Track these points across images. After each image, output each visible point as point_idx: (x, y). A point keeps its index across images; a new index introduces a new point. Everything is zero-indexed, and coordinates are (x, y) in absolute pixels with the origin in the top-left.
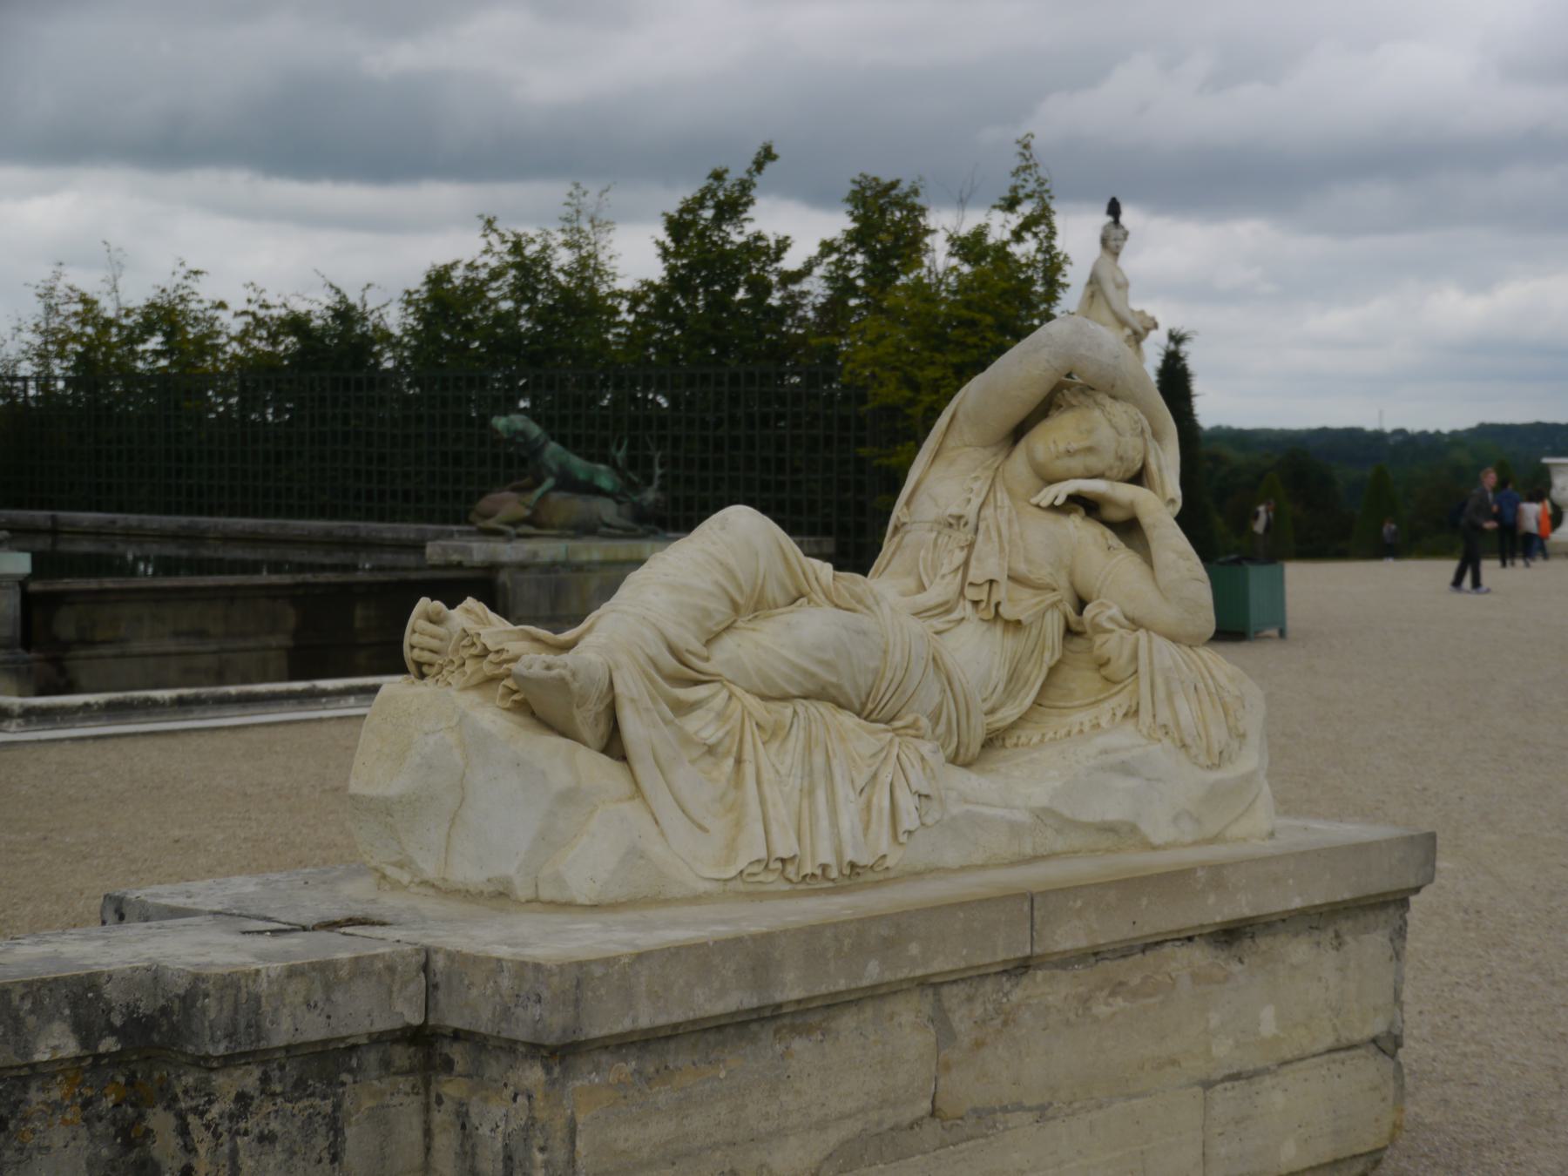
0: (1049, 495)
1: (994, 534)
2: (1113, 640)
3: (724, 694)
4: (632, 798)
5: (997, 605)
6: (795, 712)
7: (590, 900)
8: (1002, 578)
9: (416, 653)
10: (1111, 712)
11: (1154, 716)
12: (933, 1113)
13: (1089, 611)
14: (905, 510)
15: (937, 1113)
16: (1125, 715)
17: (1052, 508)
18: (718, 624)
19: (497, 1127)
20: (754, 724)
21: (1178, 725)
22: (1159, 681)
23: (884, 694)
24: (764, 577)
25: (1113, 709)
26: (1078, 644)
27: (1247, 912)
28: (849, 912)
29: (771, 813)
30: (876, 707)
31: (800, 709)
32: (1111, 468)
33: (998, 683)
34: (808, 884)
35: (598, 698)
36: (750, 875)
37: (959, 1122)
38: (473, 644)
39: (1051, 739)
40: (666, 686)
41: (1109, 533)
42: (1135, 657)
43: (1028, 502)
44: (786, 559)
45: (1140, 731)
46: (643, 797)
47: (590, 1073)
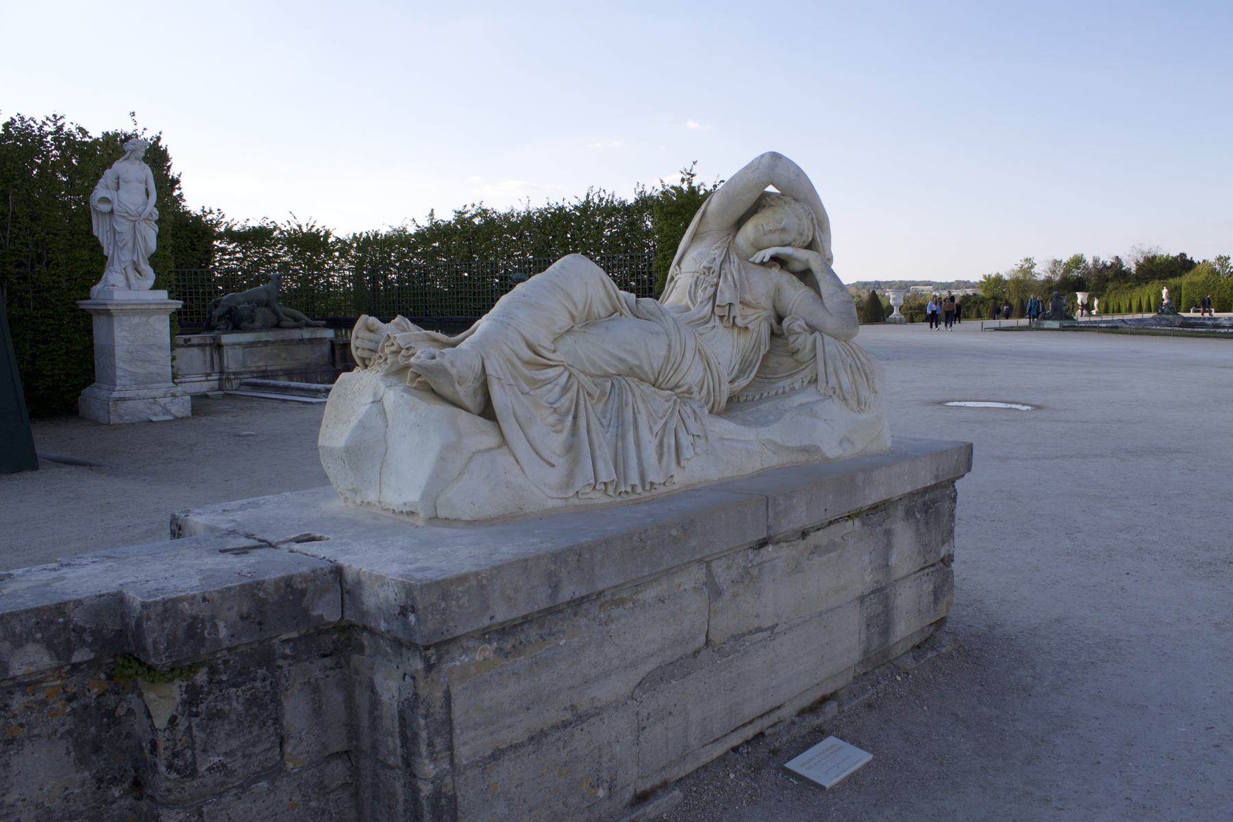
0: (758, 257)
1: (729, 277)
2: (802, 338)
3: (566, 374)
4: (500, 447)
5: (734, 318)
6: (612, 384)
7: (472, 517)
8: (736, 302)
9: (360, 352)
10: (801, 381)
11: (827, 382)
12: (708, 643)
13: (785, 323)
14: (677, 267)
15: (709, 643)
16: (809, 382)
17: (762, 264)
18: (560, 328)
19: (394, 697)
20: (586, 393)
21: (841, 387)
22: (829, 362)
23: (667, 376)
24: (591, 299)
25: (802, 378)
26: (780, 341)
27: (884, 497)
28: (649, 520)
29: (598, 453)
30: (664, 381)
31: (615, 382)
32: (795, 240)
33: (686, 384)
34: (623, 497)
35: (475, 378)
36: (583, 494)
37: (723, 645)
38: (393, 344)
39: (766, 397)
40: (523, 369)
41: (794, 278)
42: (814, 347)
43: (748, 261)
44: (605, 287)
45: (819, 391)
46: (508, 446)
47: (461, 656)
